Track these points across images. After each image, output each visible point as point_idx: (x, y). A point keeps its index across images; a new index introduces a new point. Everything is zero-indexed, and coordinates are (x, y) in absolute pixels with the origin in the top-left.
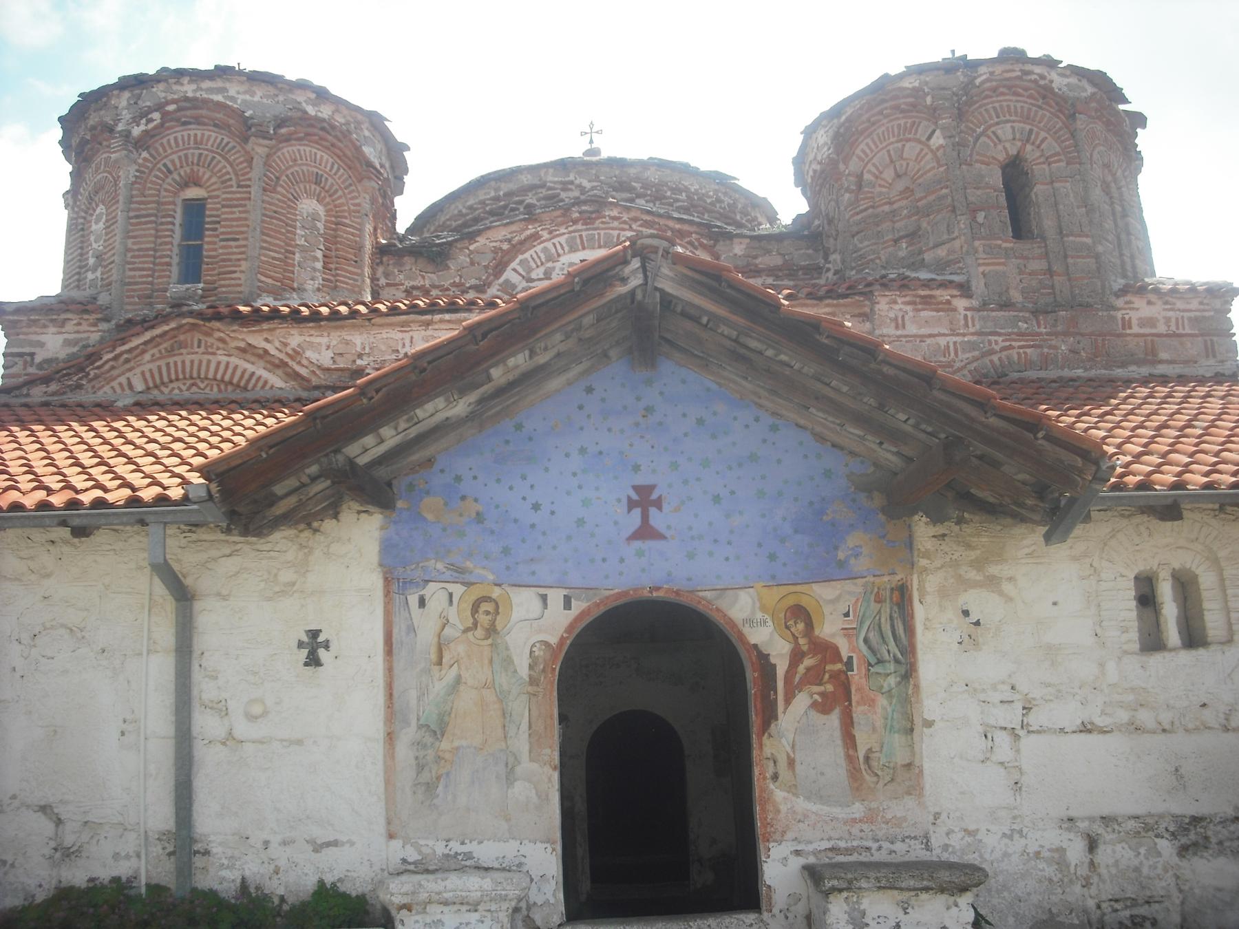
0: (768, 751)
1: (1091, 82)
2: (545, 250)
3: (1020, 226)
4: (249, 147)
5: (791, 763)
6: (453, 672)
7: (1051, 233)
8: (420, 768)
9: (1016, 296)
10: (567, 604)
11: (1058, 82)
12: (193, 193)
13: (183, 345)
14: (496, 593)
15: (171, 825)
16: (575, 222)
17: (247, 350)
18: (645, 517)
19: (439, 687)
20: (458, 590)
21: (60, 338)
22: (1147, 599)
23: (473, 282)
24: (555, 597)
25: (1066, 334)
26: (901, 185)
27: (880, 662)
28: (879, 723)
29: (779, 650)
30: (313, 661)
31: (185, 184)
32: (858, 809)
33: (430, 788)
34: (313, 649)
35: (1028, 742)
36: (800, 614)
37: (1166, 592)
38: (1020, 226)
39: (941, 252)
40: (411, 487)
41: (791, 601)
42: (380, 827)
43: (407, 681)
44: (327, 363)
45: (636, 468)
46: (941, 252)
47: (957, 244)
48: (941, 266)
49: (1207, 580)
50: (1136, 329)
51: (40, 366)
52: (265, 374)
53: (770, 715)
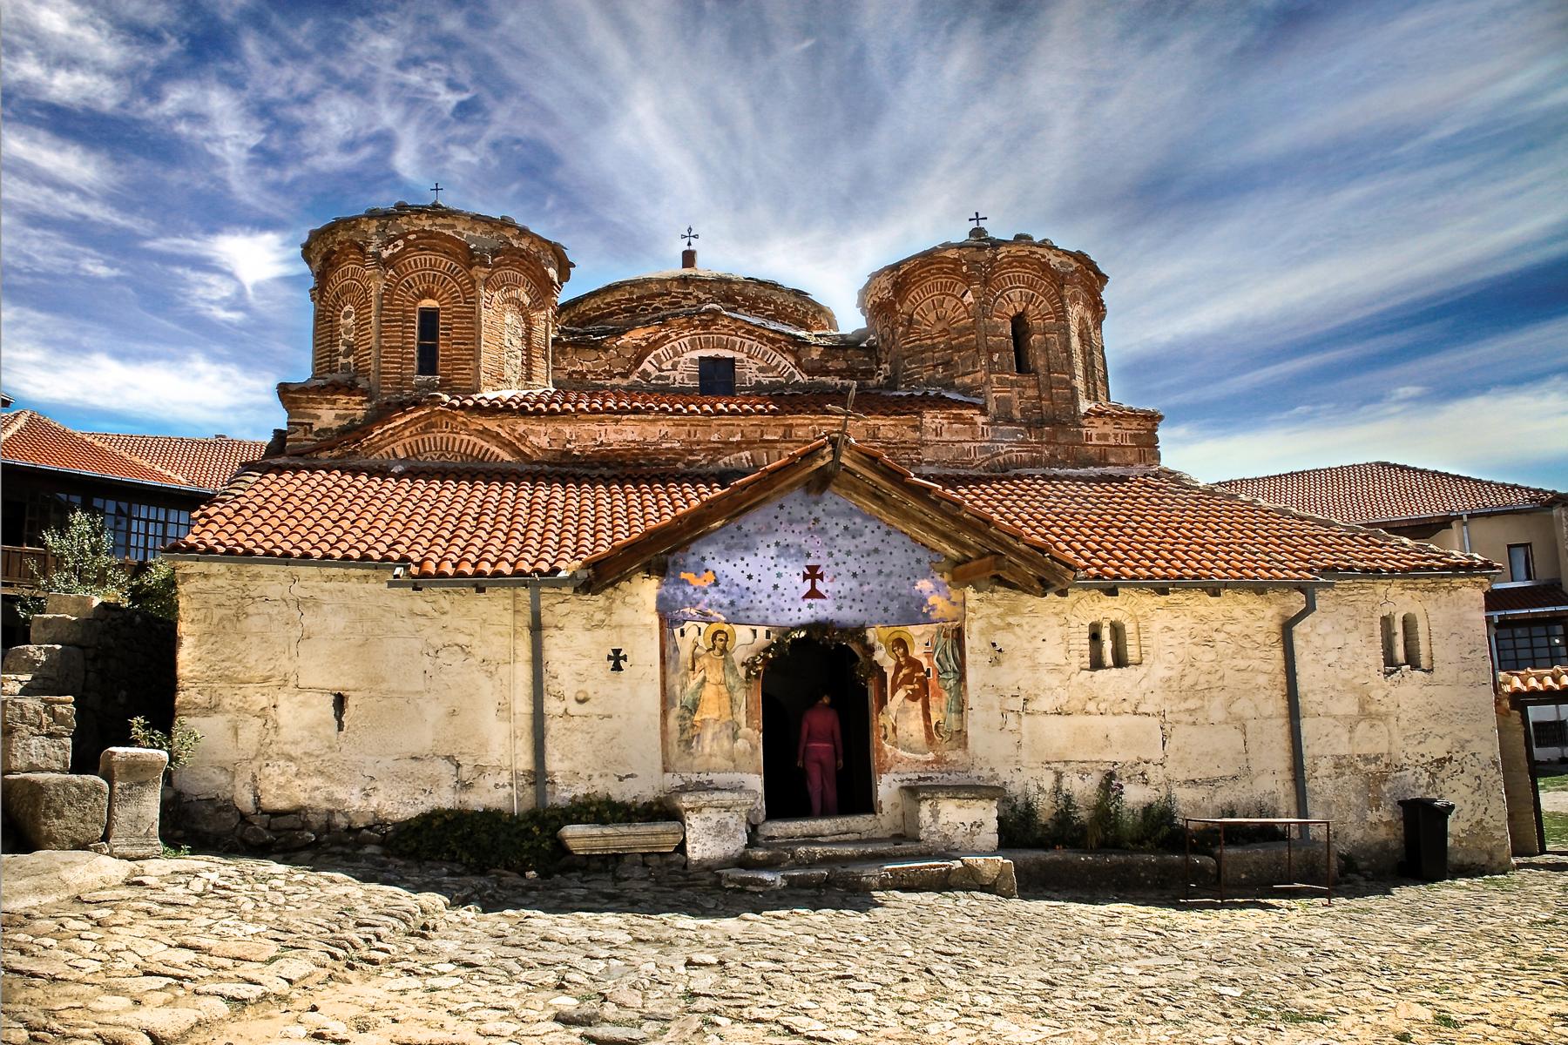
0: (881, 722)
1: (1076, 260)
2: (673, 348)
3: (1022, 366)
4: (473, 272)
5: (894, 729)
6: (700, 677)
7: (1042, 371)
8: (683, 731)
9: (1017, 414)
10: (768, 636)
11: (1054, 261)
12: (428, 303)
13: (433, 425)
14: (726, 628)
15: (530, 767)
16: (696, 327)
17: (484, 433)
18: (813, 584)
19: (693, 684)
20: (703, 626)
21: (333, 413)
22: (1095, 637)
23: (620, 370)
24: (761, 631)
25: (1048, 443)
26: (939, 327)
27: (945, 672)
28: (944, 707)
29: (889, 664)
30: (617, 668)
31: (422, 296)
32: (931, 756)
33: (688, 743)
34: (617, 660)
35: (1025, 719)
36: (901, 643)
37: (1106, 634)
38: (1022, 366)
39: (967, 380)
40: (675, 563)
41: (896, 636)
42: (659, 766)
43: (675, 680)
44: (545, 445)
45: (809, 555)
46: (967, 380)
47: (979, 375)
48: (966, 390)
49: (1130, 628)
50: (1094, 442)
51: (317, 434)
52: (497, 450)
53: (883, 701)
